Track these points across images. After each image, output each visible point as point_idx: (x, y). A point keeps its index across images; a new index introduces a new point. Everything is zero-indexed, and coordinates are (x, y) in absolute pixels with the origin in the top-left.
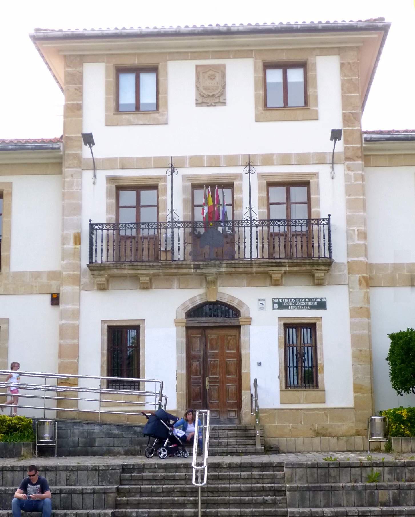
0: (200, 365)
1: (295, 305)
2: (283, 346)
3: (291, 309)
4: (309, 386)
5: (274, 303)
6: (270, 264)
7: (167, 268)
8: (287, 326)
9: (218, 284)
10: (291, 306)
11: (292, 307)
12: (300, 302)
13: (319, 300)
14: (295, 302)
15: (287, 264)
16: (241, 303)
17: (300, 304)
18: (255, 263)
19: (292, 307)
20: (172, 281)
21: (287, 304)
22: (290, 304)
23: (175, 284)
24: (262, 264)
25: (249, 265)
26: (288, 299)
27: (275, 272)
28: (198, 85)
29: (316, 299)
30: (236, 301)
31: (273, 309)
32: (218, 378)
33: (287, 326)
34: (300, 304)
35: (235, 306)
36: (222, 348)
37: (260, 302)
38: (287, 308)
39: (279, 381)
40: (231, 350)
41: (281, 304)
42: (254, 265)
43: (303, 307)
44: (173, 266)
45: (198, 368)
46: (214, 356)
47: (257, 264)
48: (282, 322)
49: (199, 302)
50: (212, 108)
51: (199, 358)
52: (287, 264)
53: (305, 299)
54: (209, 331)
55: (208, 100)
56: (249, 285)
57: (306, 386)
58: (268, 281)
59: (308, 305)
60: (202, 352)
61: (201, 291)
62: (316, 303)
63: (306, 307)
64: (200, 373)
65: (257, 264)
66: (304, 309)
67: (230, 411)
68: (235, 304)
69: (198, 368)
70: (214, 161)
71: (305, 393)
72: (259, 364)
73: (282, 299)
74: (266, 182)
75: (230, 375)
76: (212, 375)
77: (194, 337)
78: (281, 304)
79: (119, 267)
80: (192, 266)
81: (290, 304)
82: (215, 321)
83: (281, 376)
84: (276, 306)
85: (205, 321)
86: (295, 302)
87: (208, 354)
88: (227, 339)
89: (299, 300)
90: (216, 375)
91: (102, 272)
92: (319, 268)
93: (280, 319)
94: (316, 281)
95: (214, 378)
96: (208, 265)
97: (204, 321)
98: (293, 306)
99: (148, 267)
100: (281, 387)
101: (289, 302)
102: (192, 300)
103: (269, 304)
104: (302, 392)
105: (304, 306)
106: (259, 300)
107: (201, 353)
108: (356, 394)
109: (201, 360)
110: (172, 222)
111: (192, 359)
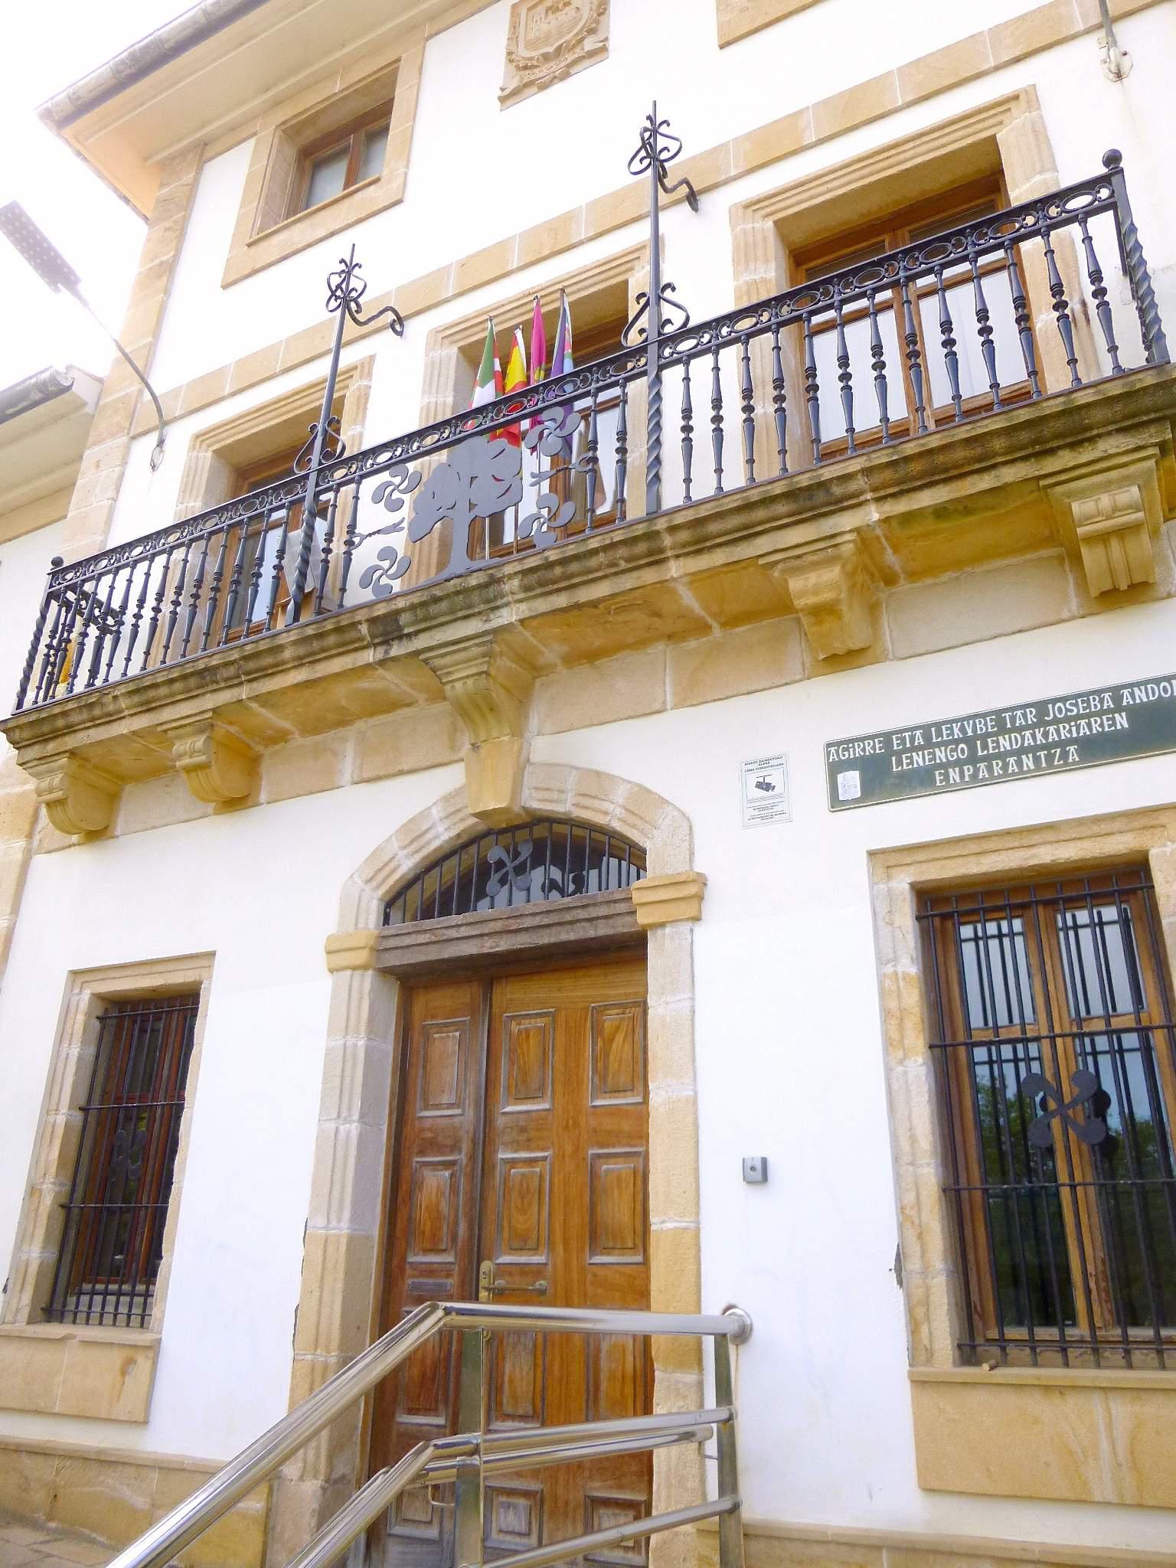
0: (454, 1188)
1: (973, 759)
2: (917, 1040)
3: (948, 788)
4: (1127, 1346)
5: (835, 769)
6: (760, 514)
7: (266, 673)
8: (946, 910)
9: (534, 723)
10: (945, 766)
11: (954, 774)
12: (1002, 730)
13: (1141, 696)
14: (970, 741)
15: (860, 483)
16: (645, 799)
17: (1005, 743)
18: (673, 529)
19: (954, 774)
20: (335, 754)
21: (919, 760)
22: (941, 755)
23: (348, 767)
24: (714, 527)
25: (642, 547)
26: (926, 728)
27: (797, 560)
28: (513, 49)
29: (1116, 691)
30: (620, 795)
31: (836, 803)
32: (538, 1271)
33: (946, 910)
34: (1005, 743)
35: (617, 825)
36: (572, 1083)
37: (753, 779)
38: (921, 782)
39: (898, 1296)
40: (616, 1091)
41: (882, 770)
42: (667, 541)
43: (1028, 762)
44: (287, 654)
45: (444, 1207)
46: (528, 1132)
47: (684, 536)
48: (902, 883)
49: (442, 834)
50: (558, 88)
51: (455, 1147)
52: (860, 483)
53: (1041, 707)
54: (511, 994)
55: (543, 72)
56: (684, 701)
57: (1127, 1346)
58: (796, 654)
59: (1063, 744)
60: (470, 1113)
61: (450, 778)
62: (1122, 721)
63: (1052, 758)
64: (454, 1238)
65: (684, 536)
66: (1038, 772)
67: (607, 1503)
68: (611, 814)
69: (444, 1207)
70: (556, 239)
71: (1122, 1410)
72: (759, 1174)
73: (886, 737)
74: (769, 224)
75: (607, 1250)
76: (513, 1250)
77: (441, 1028)
78: (882, 770)
79: (97, 712)
80: (364, 629)
81: (941, 755)
82: (514, 925)
83: (913, 1265)
84: (851, 782)
85: (464, 932)
86: (970, 741)
87: (500, 1122)
88: (597, 1030)
89: (1001, 720)
90: (535, 1250)
91: (51, 747)
92: (1086, 455)
93: (884, 859)
94: (1098, 582)
95: (523, 1269)
96: (434, 609)
97: (463, 936)
98: (959, 763)
99: (193, 682)
100: (918, 1352)
101: (929, 744)
102: (412, 831)
103: (806, 780)
104: (1096, 1404)
105: (1034, 749)
106: (749, 766)
107: (466, 1118)
108: (577, 1341)
109: (462, 1157)
110: (1053, 1039)
111: (422, 1153)
